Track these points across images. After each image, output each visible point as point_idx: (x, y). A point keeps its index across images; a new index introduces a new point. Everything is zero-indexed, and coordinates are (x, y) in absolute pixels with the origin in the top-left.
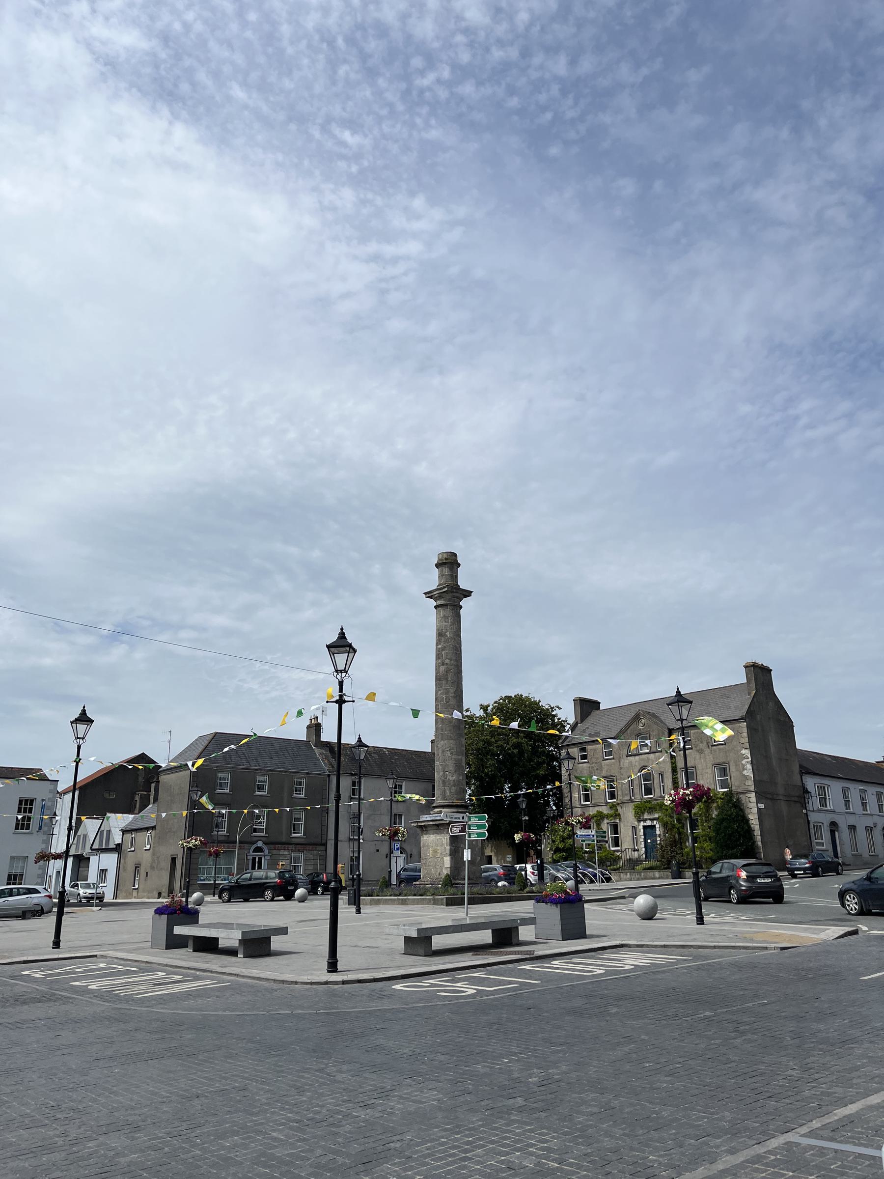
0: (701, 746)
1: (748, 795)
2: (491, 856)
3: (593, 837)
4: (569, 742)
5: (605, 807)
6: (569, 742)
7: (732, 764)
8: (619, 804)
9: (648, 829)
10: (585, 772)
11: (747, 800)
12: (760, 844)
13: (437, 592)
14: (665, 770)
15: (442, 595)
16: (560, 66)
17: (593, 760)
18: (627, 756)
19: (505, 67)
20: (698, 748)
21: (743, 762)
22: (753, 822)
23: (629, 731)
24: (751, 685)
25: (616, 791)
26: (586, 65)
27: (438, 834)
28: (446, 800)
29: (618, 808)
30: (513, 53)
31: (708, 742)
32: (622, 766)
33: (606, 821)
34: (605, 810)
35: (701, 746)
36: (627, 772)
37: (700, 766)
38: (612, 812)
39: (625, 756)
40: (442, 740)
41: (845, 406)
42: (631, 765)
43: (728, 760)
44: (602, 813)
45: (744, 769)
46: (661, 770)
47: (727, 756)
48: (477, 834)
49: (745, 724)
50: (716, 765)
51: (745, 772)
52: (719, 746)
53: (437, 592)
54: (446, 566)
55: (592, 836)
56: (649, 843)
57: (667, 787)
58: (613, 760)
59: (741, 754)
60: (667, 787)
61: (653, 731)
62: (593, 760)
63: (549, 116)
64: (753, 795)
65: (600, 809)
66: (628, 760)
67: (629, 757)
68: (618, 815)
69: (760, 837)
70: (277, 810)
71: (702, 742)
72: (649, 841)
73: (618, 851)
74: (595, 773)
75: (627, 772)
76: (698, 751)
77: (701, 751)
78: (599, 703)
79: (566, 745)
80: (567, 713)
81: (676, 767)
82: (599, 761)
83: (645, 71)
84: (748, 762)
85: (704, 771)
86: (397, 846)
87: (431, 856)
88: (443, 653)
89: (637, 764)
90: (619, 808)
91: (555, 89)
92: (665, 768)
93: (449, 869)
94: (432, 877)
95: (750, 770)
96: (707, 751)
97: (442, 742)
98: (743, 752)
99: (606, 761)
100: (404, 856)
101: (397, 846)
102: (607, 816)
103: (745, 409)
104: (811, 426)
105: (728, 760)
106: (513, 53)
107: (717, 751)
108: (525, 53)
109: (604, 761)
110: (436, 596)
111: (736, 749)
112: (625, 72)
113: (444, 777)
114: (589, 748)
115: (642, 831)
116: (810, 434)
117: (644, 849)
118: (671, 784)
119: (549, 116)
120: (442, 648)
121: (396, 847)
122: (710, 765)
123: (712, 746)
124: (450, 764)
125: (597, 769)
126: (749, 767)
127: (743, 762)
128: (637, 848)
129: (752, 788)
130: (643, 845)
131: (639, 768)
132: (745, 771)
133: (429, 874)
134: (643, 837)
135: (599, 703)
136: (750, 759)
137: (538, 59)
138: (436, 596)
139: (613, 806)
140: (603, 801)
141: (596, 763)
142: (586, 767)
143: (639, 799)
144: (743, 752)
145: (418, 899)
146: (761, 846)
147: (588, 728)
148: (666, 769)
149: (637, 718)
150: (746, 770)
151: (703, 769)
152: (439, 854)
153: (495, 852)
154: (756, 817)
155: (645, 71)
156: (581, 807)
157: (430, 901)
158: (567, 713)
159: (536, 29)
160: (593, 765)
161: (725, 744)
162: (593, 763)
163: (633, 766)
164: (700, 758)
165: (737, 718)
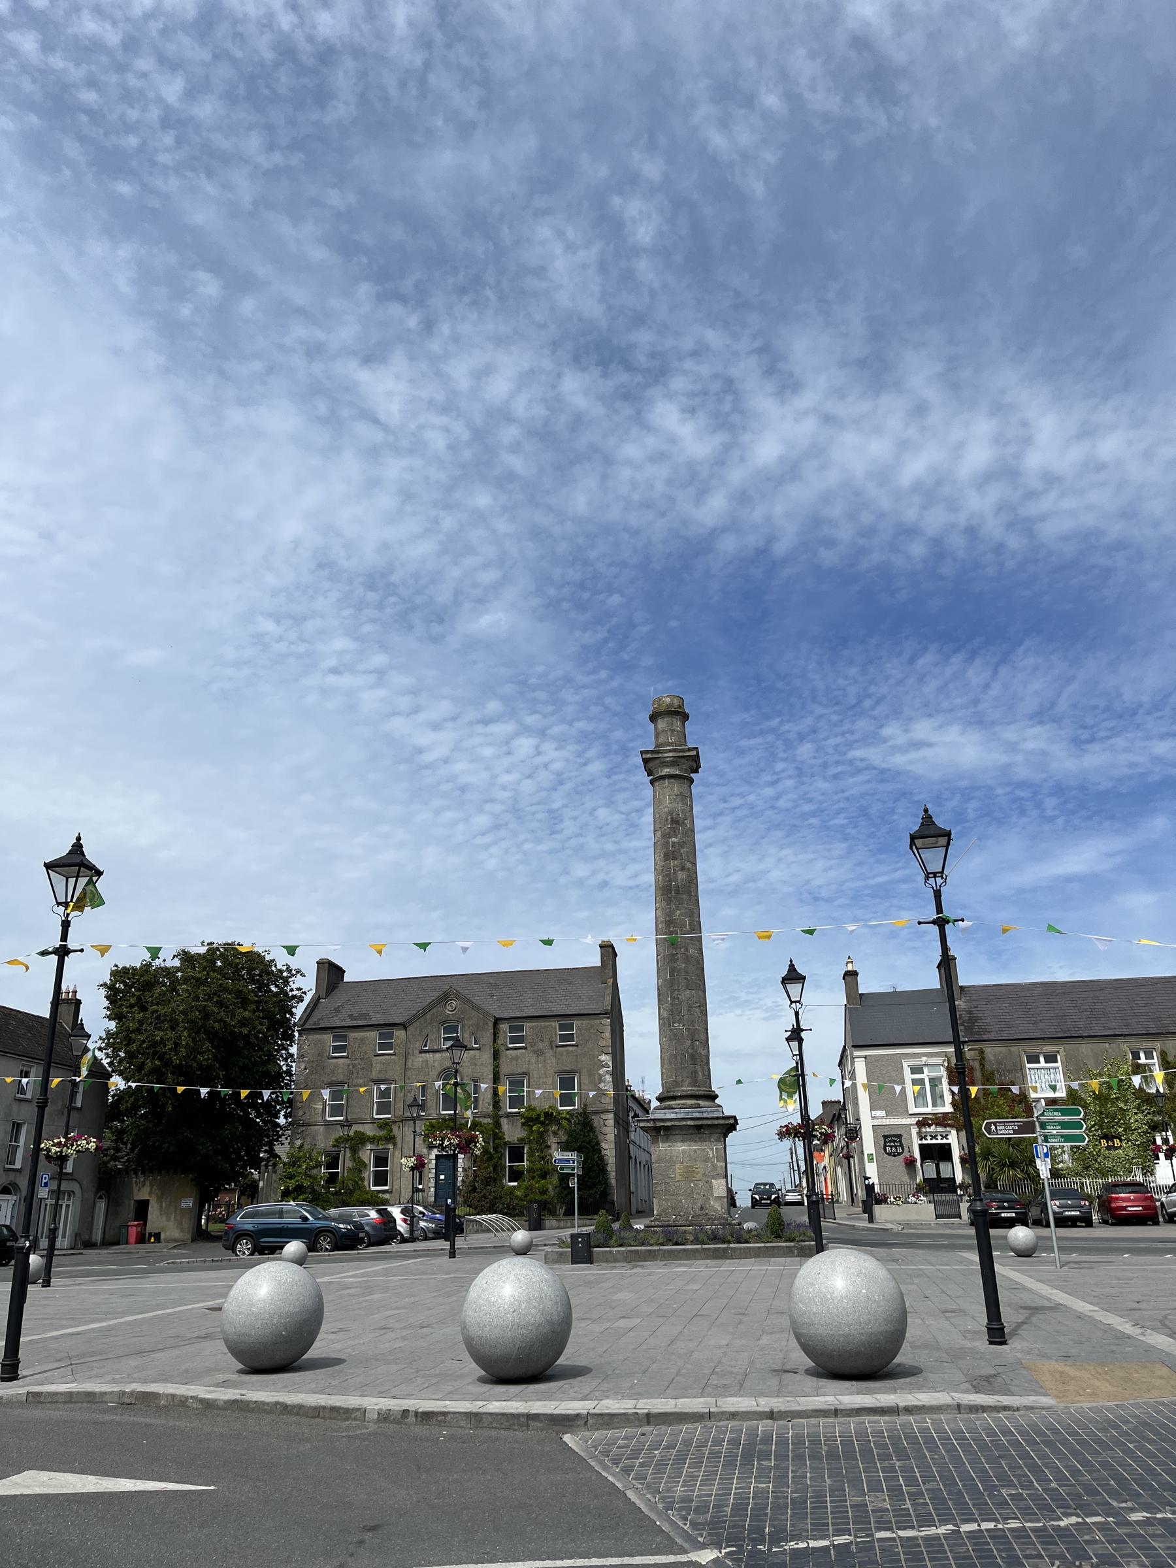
0: (541, 1045)
1: (604, 1116)
2: (147, 1201)
3: (574, 1163)
4: (314, 1024)
5: (370, 1125)
6: (314, 1024)
7: (584, 1072)
8: (396, 1122)
9: (442, 1160)
10: (340, 1071)
11: (602, 1123)
12: (613, 1182)
13: (671, 754)
14: (482, 1075)
15: (679, 760)
16: (172, 89)
17: (357, 1055)
18: (420, 1052)
19: (88, 49)
20: (536, 1048)
21: (601, 1072)
22: (607, 1152)
23: (428, 1016)
24: (606, 971)
25: (393, 1104)
26: (206, 109)
27: (695, 1141)
28: (699, 1086)
29: (393, 1127)
30: (113, 37)
31: (552, 1041)
32: (410, 1066)
33: (369, 1147)
34: (369, 1130)
35: (541, 1045)
36: (416, 1075)
37: (535, 1072)
38: (382, 1133)
39: (417, 1052)
40: (687, 988)
41: (379, 659)
42: (427, 1064)
43: (580, 1066)
44: (363, 1134)
45: (601, 1081)
46: (475, 1074)
47: (577, 1062)
48: (1062, 1136)
49: (609, 1020)
50: (559, 1073)
51: (602, 1086)
52: (568, 1048)
53: (671, 754)
54: (678, 717)
55: (571, 1162)
56: (442, 1180)
57: (483, 1100)
58: (393, 1057)
59: (600, 1060)
60: (483, 1100)
61: (469, 1019)
62: (357, 1055)
63: (133, 141)
64: (611, 1116)
65: (359, 1128)
66: (422, 1057)
67: (423, 1054)
68: (391, 1139)
69: (614, 1174)
70: (204, 1091)
71: (542, 1041)
72: (442, 1177)
73: (384, 1192)
74: (358, 1073)
75: (416, 1075)
76: (535, 1052)
77: (539, 1053)
78: (344, 971)
79: (308, 1029)
80: (306, 984)
81: (498, 1072)
82: (367, 1056)
83: (278, 158)
84: (607, 1072)
85: (542, 1080)
86: (45, 1178)
87: (678, 1178)
88: (682, 851)
89: (436, 1064)
90: (395, 1128)
91: (154, 114)
92: (483, 1073)
93: (725, 1200)
94: (682, 1214)
95: (609, 1082)
96: (549, 1053)
97: (688, 992)
98: (603, 1058)
99: (381, 1057)
100: (15, 1198)
101: (45, 1178)
102: (373, 1140)
103: (268, 626)
104: (335, 671)
105: (580, 1066)
106: (113, 37)
107: (565, 1054)
108: (131, 45)
109: (377, 1058)
110: (668, 759)
111: (591, 1053)
112: (253, 143)
113: (693, 1049)
114: (352, 1035)
115: (434, 1162)
116: (332, 680)
117: (433, 1189)
118: (489, 1096)
119: (133, 141)
120: (679, 843)
121: (44, 1181)
122: (550, 1072)
123: (557, 1047)
124: (700, 1029)
125: (363, 1068)
126: (608, 1078)
127: (601, 1072)
128: (420, 1187)
129: (611, 1107)
130: (432, 1183)
131: (440, 1070)
132: (603, 1084)
133: (674, 1209)
134: (434, 1171)
135: (344, 971)
136: (611, 1069)
137: (145, 63)
138: (668, 759)
139: (384, 1125)
140: (320, 1119)
141: (362, 1059)
142: (343, 1064)
143: (434, 1115)
144: (603, 1058)
145: (759, 1248)
146: (614, 1184)
147: (342, 1006)
148: (485, 1074)
149: (445, 998)
150: (604, 1082)
151: (540, 1077)
152: (700, 1174)
153: (157, 1194)
154: (613, 1145)
155: (278, 158)
156: (325, 1125)
157: (792, 1252)
158: (306, 984)
159: (155, 26)
160: (356, 1062)
161: (577, 1046)
162: (356, 1059)
163: (430, 1066)
164: (537, 1063)
165: (598, 1012)
